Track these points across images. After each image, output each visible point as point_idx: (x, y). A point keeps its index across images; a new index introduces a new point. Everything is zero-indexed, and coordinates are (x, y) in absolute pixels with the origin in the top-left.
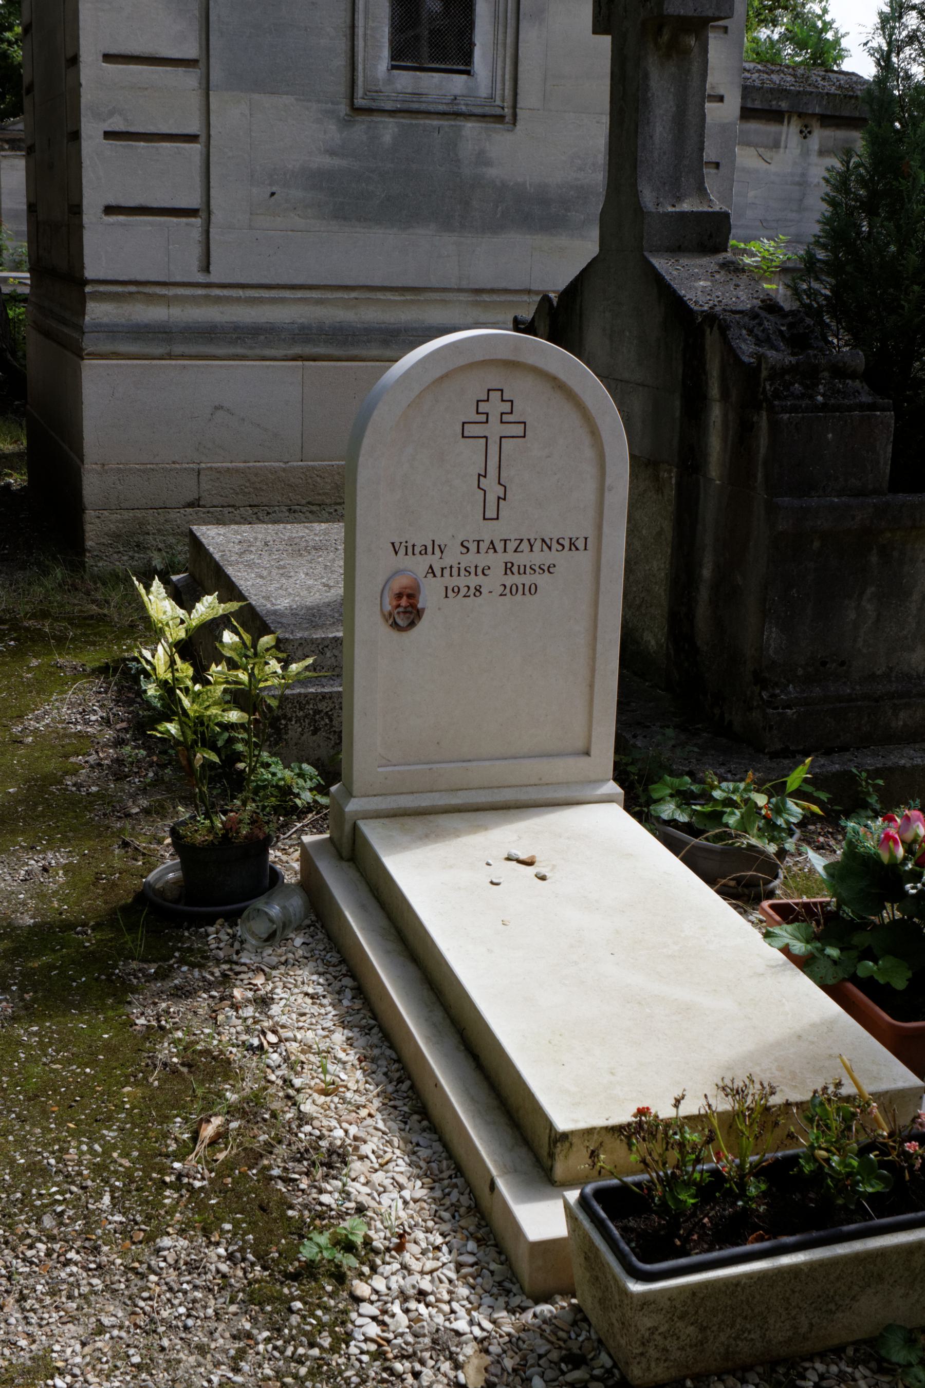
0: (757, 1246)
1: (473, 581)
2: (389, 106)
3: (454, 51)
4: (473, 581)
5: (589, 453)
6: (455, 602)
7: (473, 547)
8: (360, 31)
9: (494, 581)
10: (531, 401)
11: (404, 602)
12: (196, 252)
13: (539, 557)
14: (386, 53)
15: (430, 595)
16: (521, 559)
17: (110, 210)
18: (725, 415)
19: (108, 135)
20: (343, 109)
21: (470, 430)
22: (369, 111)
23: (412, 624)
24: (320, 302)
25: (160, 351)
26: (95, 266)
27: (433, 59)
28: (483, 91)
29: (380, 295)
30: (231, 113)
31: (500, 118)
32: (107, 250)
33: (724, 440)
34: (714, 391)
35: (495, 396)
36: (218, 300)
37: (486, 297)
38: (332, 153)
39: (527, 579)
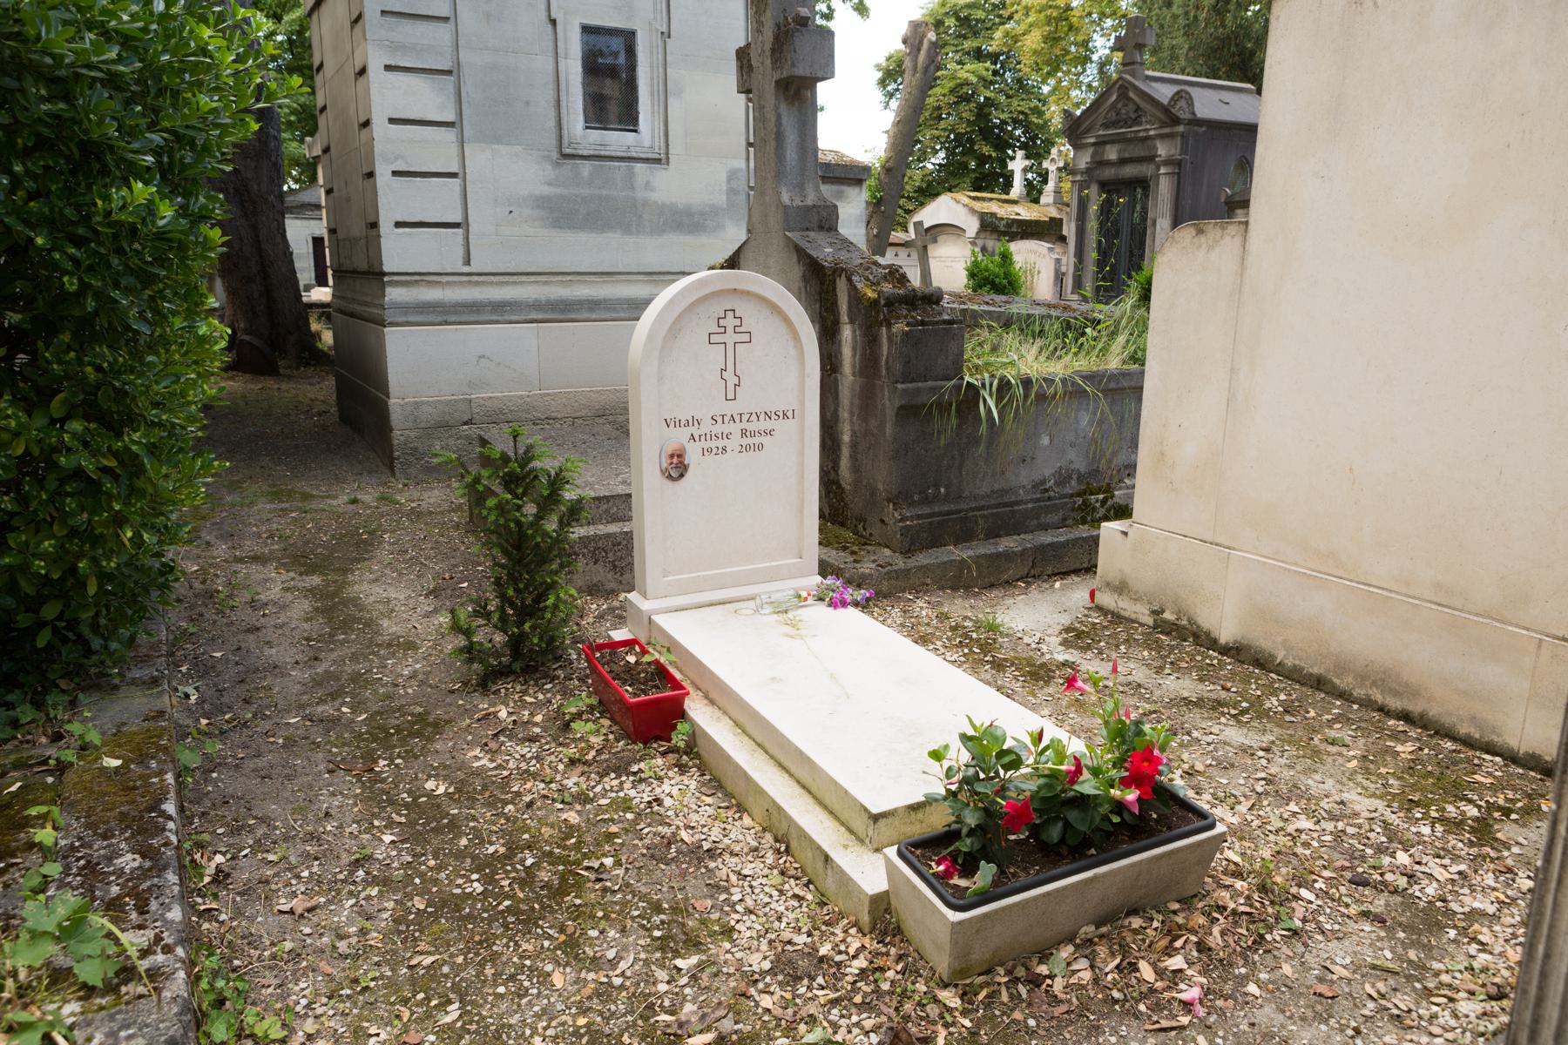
0: (1069, 867)
1: (721, 443)
2: (586, 153)
3: (628, 119)
4: (721, 443)
5: (793, 352)
6: (710, 458)
7: (720, 420)
8: (563, 104)
9: (734, 443)
10: (754, 318)
11: (675, 460)
12: (461, 252)
13: (764, 425)
14: (581, 118)
15: (693, 456)
16: (751, 427)
17: (398, 225)
18: (854, 337)
19: (395, 173)
20: (555, 155)
21: (714, 338)
22: (573, 156)
23: (682, 476)
24: (546, 283)
25: (439, 319)
26: (392, 260)
27: (620, 122)
28: (647, 144)
29: (587, 278)
30: (479, 159)
31: (658, 161)
32: (396, 252)
33: (854, 349)
34: (845, 318)
35: (730, 314)
36: (477, 283)
37: (655, 277)
38: (550, 184)
39: (757, 440)
